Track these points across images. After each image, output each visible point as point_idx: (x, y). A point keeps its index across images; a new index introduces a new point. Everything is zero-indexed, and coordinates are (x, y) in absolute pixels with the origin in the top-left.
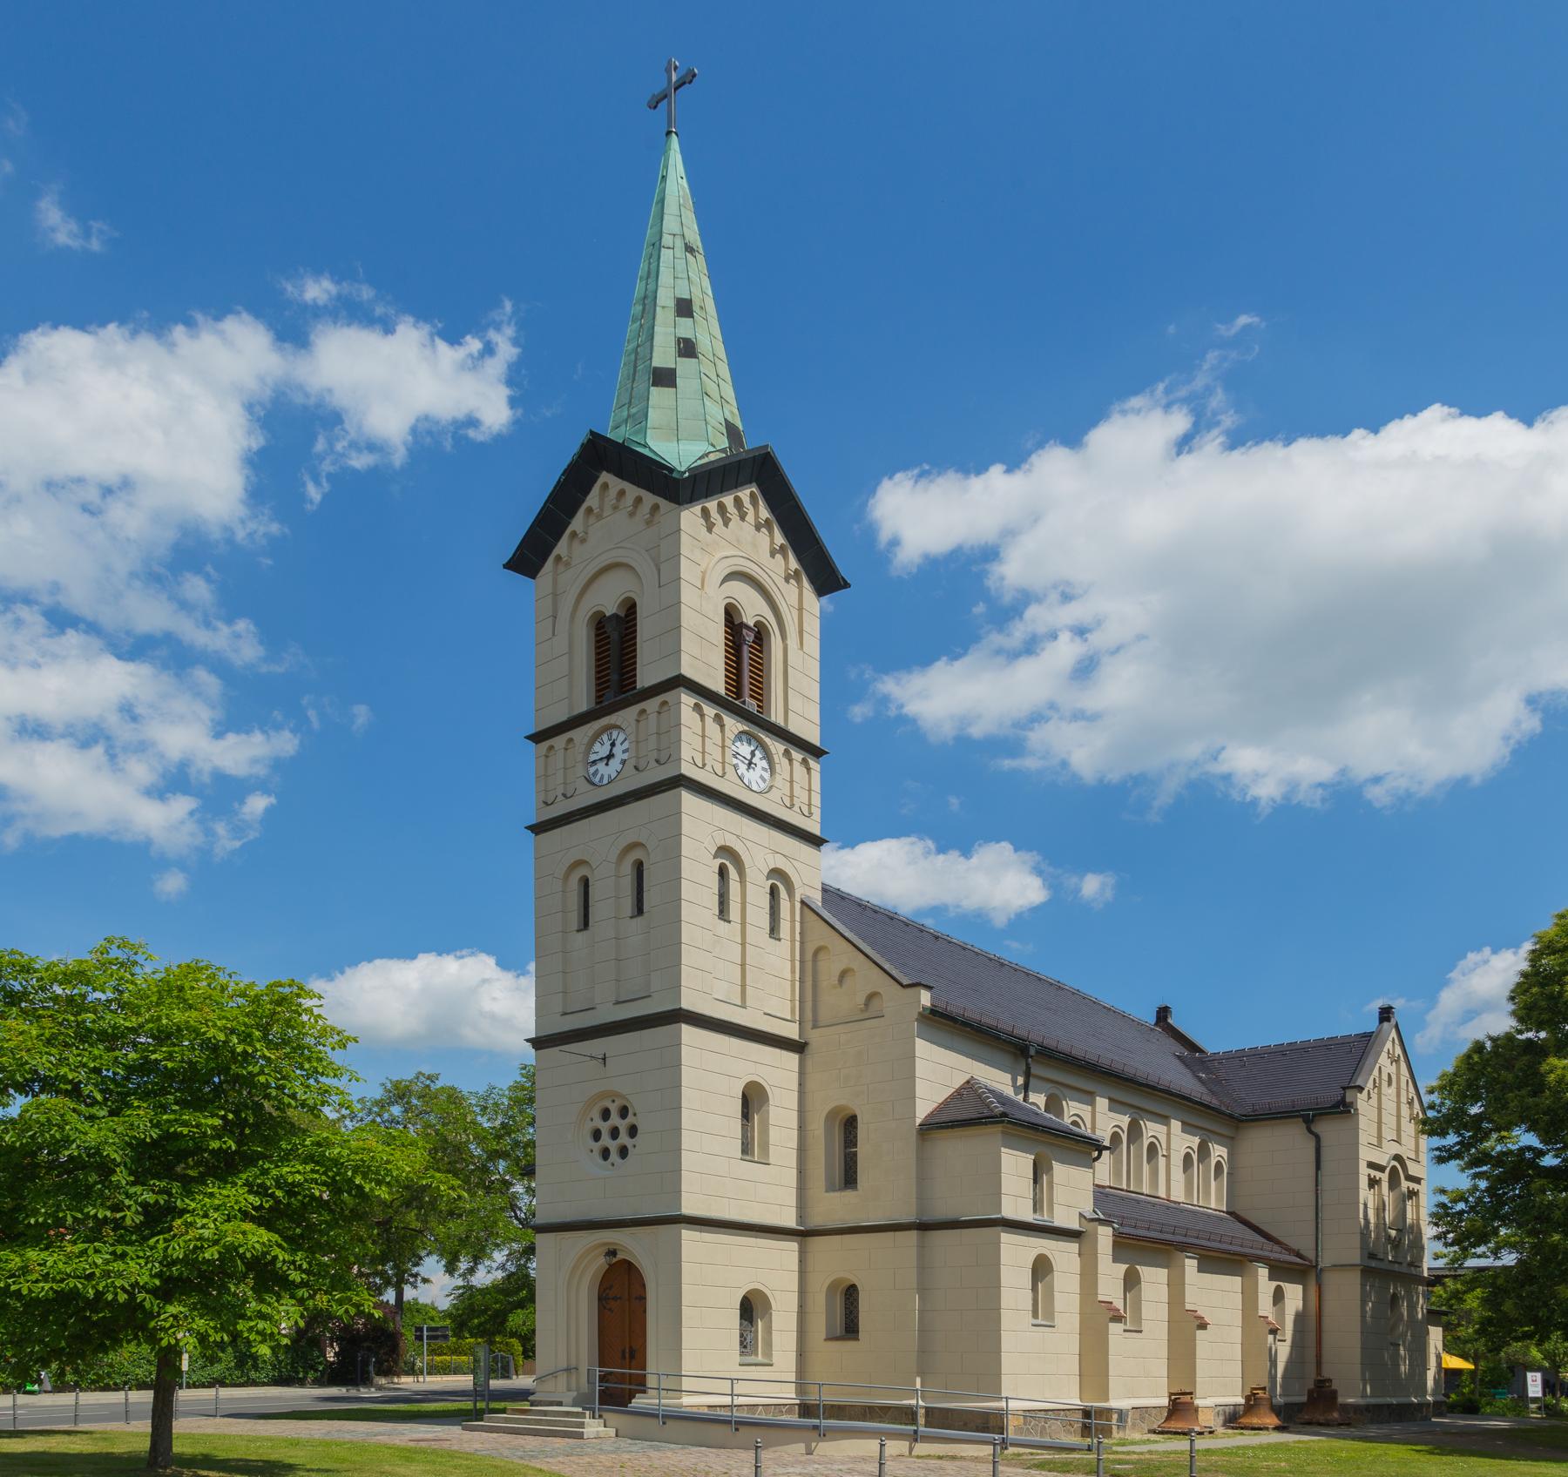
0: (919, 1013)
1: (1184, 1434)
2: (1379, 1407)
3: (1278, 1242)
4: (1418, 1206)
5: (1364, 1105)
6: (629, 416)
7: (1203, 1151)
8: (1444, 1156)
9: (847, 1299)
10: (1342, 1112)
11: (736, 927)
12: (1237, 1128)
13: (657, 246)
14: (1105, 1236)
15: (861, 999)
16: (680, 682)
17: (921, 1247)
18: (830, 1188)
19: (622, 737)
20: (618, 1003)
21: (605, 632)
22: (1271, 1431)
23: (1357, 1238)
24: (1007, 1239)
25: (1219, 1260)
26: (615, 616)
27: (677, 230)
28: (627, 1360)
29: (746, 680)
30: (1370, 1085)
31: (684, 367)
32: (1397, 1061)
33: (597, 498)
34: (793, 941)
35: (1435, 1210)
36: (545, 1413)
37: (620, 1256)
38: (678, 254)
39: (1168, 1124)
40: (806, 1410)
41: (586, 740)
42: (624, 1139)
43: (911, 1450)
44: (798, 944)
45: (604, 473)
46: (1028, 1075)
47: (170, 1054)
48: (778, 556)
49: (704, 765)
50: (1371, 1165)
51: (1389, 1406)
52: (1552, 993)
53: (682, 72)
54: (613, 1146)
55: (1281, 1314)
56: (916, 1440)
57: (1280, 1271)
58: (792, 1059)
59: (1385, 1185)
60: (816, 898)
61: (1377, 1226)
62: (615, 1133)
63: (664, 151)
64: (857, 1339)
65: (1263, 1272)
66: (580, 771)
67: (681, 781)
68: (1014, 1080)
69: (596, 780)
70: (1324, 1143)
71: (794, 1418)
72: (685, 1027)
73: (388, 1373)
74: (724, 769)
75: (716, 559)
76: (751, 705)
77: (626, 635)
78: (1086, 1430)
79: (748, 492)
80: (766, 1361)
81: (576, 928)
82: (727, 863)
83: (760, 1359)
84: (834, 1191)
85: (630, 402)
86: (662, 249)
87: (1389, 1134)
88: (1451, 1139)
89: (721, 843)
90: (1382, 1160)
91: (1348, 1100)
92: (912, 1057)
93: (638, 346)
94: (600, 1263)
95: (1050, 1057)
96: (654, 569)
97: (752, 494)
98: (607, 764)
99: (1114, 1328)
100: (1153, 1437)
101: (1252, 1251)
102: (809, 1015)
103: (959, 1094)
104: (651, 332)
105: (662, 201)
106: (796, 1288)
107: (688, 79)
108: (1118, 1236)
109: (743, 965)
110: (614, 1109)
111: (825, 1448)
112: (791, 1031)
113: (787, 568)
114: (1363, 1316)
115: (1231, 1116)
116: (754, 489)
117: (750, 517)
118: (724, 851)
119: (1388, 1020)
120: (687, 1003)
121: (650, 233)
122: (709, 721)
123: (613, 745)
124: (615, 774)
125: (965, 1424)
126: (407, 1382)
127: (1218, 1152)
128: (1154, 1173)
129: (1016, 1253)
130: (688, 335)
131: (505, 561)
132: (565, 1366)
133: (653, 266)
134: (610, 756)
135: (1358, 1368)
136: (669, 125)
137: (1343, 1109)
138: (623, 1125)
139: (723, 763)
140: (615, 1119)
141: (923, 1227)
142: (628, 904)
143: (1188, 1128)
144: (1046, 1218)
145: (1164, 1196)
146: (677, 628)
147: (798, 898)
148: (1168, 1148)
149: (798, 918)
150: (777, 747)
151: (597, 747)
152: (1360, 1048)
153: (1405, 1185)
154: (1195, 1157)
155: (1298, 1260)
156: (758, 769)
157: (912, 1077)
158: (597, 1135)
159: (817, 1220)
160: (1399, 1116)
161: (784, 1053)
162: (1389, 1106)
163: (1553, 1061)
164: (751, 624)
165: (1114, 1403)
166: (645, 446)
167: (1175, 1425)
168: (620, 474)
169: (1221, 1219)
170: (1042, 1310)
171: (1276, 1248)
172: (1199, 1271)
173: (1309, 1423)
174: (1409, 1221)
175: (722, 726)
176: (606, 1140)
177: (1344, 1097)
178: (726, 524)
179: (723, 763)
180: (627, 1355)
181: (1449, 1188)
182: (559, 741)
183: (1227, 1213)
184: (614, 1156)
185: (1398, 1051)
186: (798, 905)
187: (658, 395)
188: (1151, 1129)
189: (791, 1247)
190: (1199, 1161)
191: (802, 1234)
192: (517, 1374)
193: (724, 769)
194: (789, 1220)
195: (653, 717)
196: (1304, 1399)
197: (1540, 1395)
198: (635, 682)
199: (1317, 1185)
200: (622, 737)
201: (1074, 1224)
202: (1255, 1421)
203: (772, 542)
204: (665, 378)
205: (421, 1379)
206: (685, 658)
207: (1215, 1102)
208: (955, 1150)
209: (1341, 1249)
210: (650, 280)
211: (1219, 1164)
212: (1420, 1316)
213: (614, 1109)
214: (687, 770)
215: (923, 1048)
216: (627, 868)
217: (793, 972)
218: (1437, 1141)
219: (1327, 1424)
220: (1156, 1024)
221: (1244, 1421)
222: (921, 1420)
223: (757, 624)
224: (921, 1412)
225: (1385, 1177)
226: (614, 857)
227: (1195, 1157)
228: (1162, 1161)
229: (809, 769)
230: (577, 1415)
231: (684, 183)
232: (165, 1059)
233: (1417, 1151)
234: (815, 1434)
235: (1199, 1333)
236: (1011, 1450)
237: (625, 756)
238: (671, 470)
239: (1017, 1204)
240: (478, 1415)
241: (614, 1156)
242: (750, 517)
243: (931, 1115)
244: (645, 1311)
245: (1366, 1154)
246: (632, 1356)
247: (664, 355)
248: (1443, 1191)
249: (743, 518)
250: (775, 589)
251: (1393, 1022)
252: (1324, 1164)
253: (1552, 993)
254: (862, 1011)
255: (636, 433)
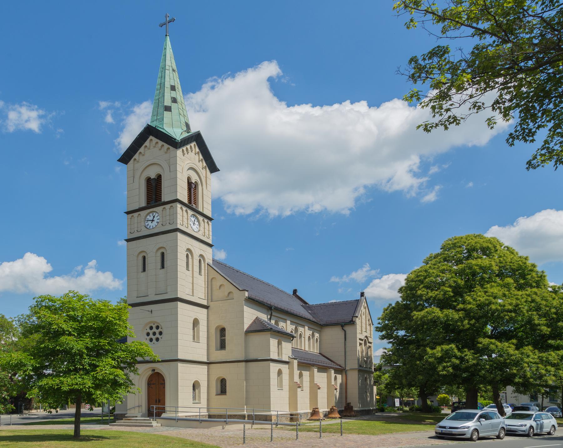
0: (245, 299)
1: (317, 420)
2: (363, 411)
3: (334, 362)
4: (371, 351)
5: (358, 321)
6: (157, 119)
7: (313, 335)
8: (383, 338)
9: (221, 383)
10: (352, 324)
11: (191, 272)
12: (321, 328)
13: (164, 69)
14: (295, 362)
15: (226, 294)
16: (177, 201)
17: (246, 367)
18: (217, 350)
19: (157, 215)
20: (156, 295)
21: (150, 182)
22: (338, 419)
23: (357, 360)
24: (272, 365)
25: (323, 369)
26: (154, 179)
27: (170, 65)
28: (158, 403)
29: (193, 199)
30: (359, 316)
31: (174, 106)
32: (365, 308)
33: (149, 143)
34: (205, 275)
35: (383, 354)
36: (137, 420)
37: (156, 371)
38: (171, 72)
39: (304, 328)
40: (210, 416)
41: (145, 215)
42: (157, 335)
43: (252, 427)
44: (206, 277)
45: (151, 136)
46: (271, 315)
47: (94, 323)
48: (201, 162)
49: (183, 225)
50: (360, 339)
51: (365, 410)
52: (413, 293)
53: (171, 18)
54: (154, 338)
55: (336, 383)
56: (253, 424)
57: (338, 371)
58: (205, 311)
59: (363, 345)
60: (211, 262)
61: (361, 356)
62: (154, 334)
63: (165, 40)
64: (226, 395)
65: (333, 371)
66: (143, 224)
67: (177, 230)
68: (267, 317)
69: (148, 227)
70: (347, 332)
71: (207, 419)
72: (179, 303)
73: (27, 409)
74: (188, 225)
75: (186, 164)
76: (194, 206)
77: (157, 184)
78: (292, 419)
79: (193, 144)
80: (199, 402)
81: (141, 271)
82: (188, 253)
83: (197, 401)
84: (218, 350)
85: (157, 115)
86: (166, 70)
87: (364, 330)
88: (384, 333)
89: (187, 248)
90: (363, 338)
91: (354, 320)
92: (243, 311)
93: (159, 98)
94: (150, 373)
95: (277, 310)
96: (169, 167)
97: (194, 144)
98: (152, 223)
99: (299, 390)
100: (309, 421)
101: (313, 363)
102: (210, 298)
103: (254, 322)
104: (163, 94)
105: (165, 55)
106: (207, 380)
107: (173, 20)
108: (299, 362)
109: (193, 283)
110: (154, 327)
111: (228, 427)
112: (205, 303)
113: (203, 166)
114: (359, 384)
115: (320, 325)
116: (195, 143)
117: (194, 151)
118: (189, 250)
119: (363, 296)
120: (180, 295)
121: (161, 64)
122: (184, 212)
123: (154, 217)
124: (155, 226)
125: (260, 419)
126: (34, 411)
127: (317, 335)
128: (301, 342)
129: (274, 368)
130: (175, 96)
131: (118, 159)
132: (138, 405)
133: (163, 75)
134: (153, 221)
135: (357, 399)
136: (167, 33)
137: (352, 323)
138: (157, 331)
139: (188, 224)
140: (154, 330)
141: (247, 361)
142: (159, 265)
143: (310, 328)
144: (280, 358)
145: (303, 349)
146: (176, 185)
147: (206, 263)
148: (305, 335)
149: (206, 269)
150: (201, 218)
151: (148, 217)
152: (356, 303)
153: (368, 344)
154: (311, 337)
155: (340, 368)
156: (196, 225)
157: (243, 317)
158: (148, 334)
159: (212, 359)
160: (366, 324)
161: (203, 309)
162: (364, 321)
163: (415, 312)
164: (194, 182)
165: (299, 411)
166: (163, 129)
167: (314, 418)
168: (156, 137)
169: (319, 356)
170: (280, 385)
171: (333, 364)
172: (318, 372)
173: (345, 416)
174: (369, 355)
175: (187, 213)
176: (151, 336)
177: (352, 319)
178: (188, 154)
179: (188, 224)
180: (158, 401)
181: (387, 348)
182: (136, 215)
183: (319, 353)
184: (154, 341)
185: (366, 305)
186: (206, 265)
187: (166, 114)
188: (301, 329)
189: (205, 367)
190: (312, 338)
191: (208, 364)
192: (68, 408)
193: (188, 225)
194: (205, 360)
195: (168, 210)
196: (343, 409)
197: (399, 405)
198: (161, 200)
199: (345, 345)
200: (157, 215)
201: (287, 360)
202: (333, 416)
203: (199, 158)
204: (168, 109)
205: (39, 411)
206: (178, 194)
207: (314, 320)
208: (256, 338)
209: (352, 364)
210: (162, 79)
211: (317, 339)
212: (372, 383)
213: (154, 327)
214: (179, 227)
215: (246, 308)
216: (159, 254)
217: (205, 285)
218: (381, 334)
219: (351, 416)
220: (293, 295)
221: (330, 416)
222: (246, 418)
223: (195, 182)
224: (246, 416)
225: (363, 342)
226: (155, 251)
227: (311, 337)
228: (303, 338)
229: (209, 224)
230: (148, 420)
231: (171, 50)
232: (93, 325)
233: (370, 334)
234: (225, 423)
235: (319, 390)
236: (279, 426)
237: (158, 221)
238: (175, 139)
239: (274, 355)
240: (114, 421)
241: (154, 341)
242: (194, 151)
243: (248, 328)
244: (164, 387)
245: (359, 336)
246: (159, 401)
247: (168, 102)
248: (386, 349)
249: (192, 152)
250: (200, 172)
251: (364, 297)
252: (347, 339)
253: (413, 293)
254: (227, 297)
255: (160, 124)
